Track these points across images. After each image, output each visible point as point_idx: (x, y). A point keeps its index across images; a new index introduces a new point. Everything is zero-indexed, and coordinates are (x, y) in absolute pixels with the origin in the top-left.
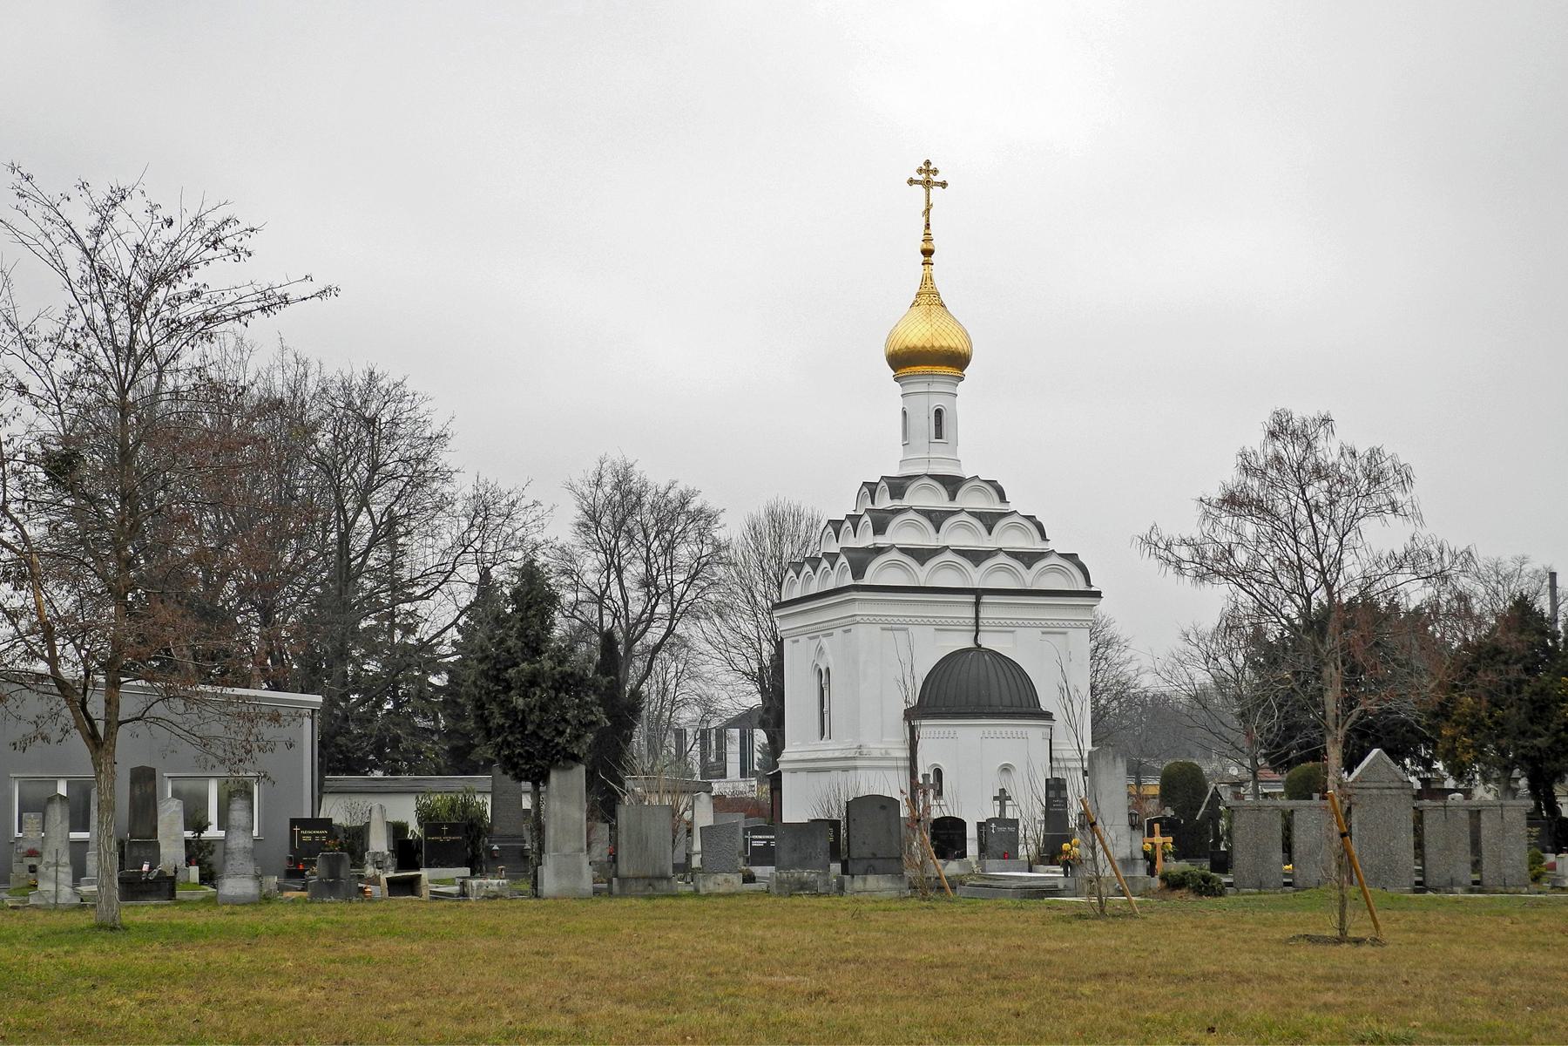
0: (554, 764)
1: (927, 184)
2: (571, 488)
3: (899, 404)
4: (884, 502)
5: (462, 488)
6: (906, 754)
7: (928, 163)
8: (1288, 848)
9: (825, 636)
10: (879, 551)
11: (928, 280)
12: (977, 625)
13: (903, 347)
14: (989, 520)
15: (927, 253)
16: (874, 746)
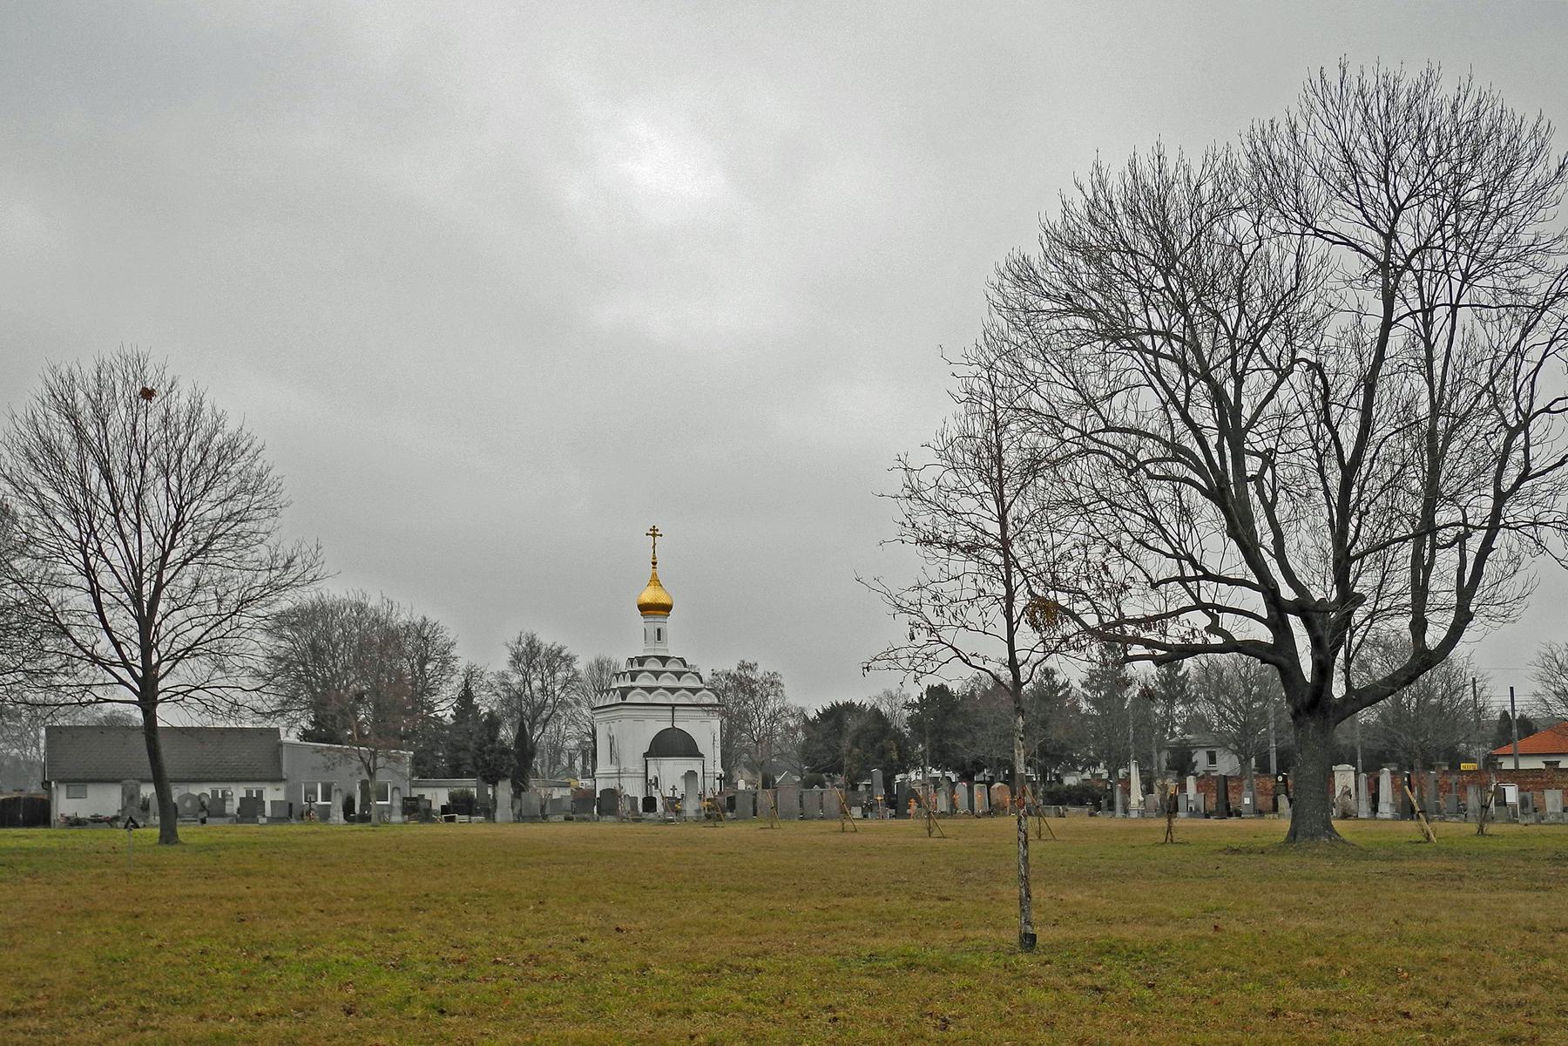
0: (500, 778)
1: (654, 535)
2: (507, 645)
3: (644, 626)
4: (636, 668)
5: (461, 665)
8: (822, 807)
10: (633, 688)
14: (679, 675)
15: (654, 563)
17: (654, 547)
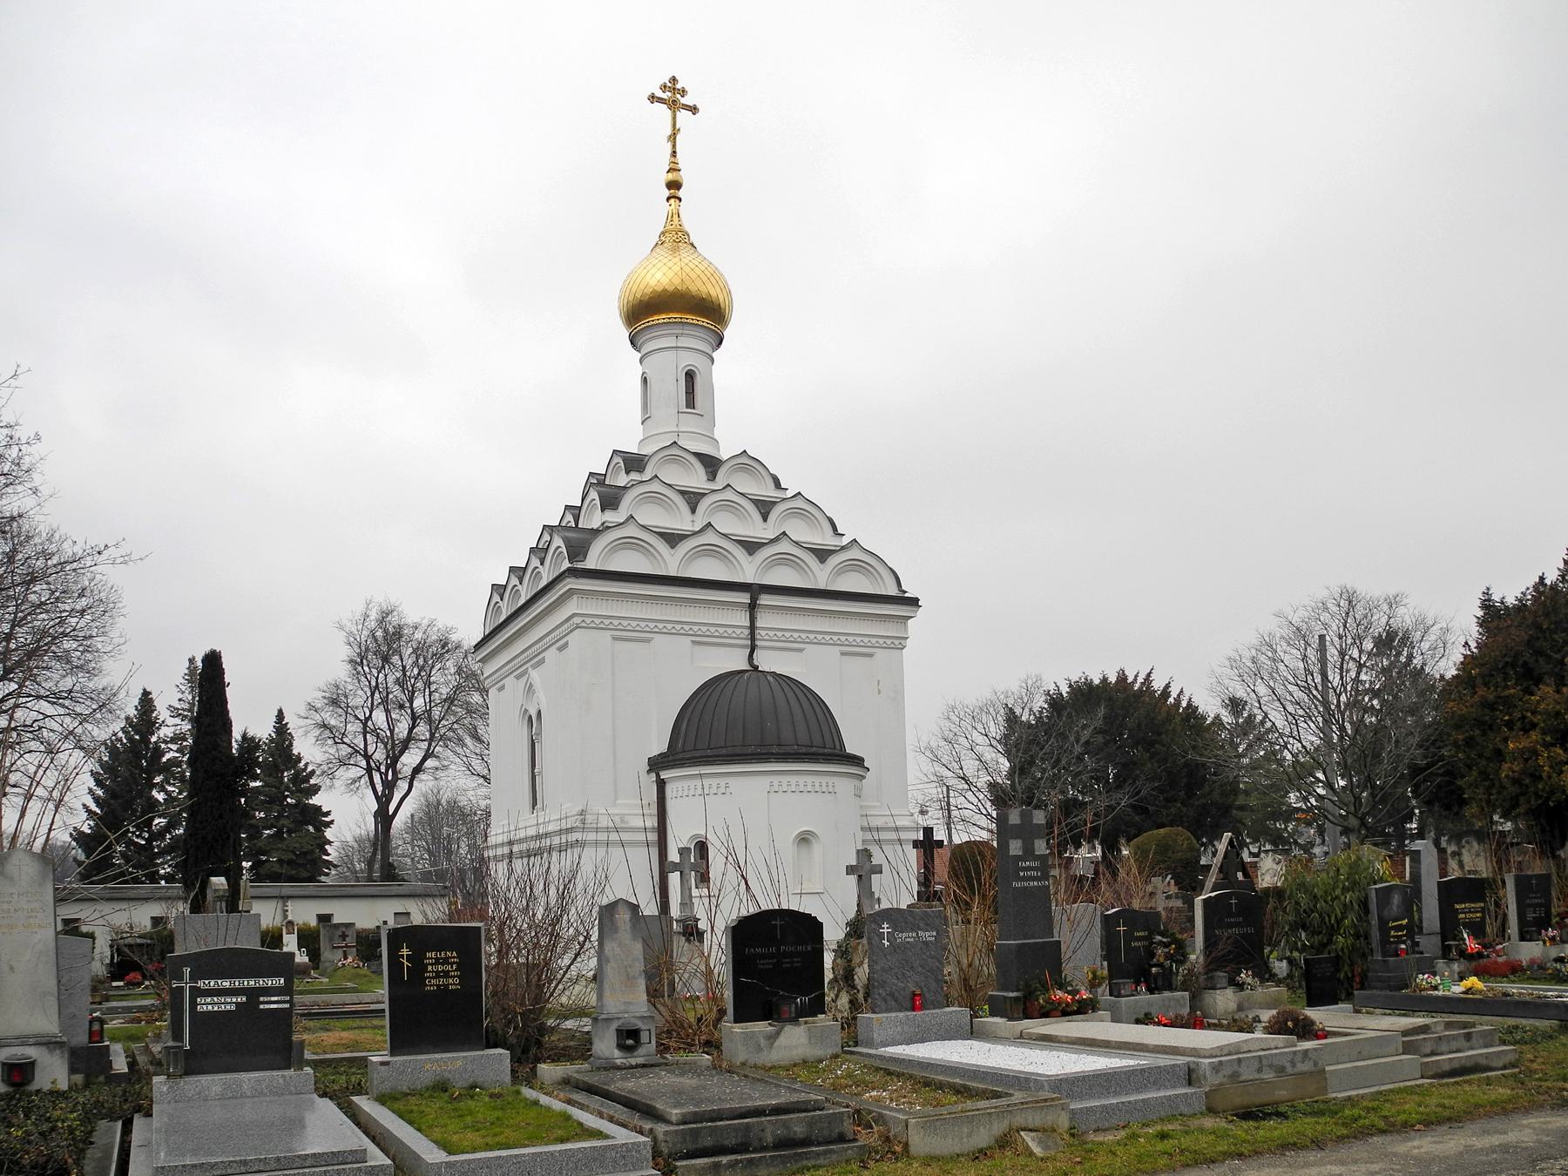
1: (673, 105)
2: (341, 628)
3: (638, 370)
6: (652, 822)
7: (674, 80)
9: (535, 667)
11: (675, 217)
12: (753, 637)
13: (648, 291)
14: (765, 508)
15: (674, 185)
16: (603, 811)
17: (673, 138)
